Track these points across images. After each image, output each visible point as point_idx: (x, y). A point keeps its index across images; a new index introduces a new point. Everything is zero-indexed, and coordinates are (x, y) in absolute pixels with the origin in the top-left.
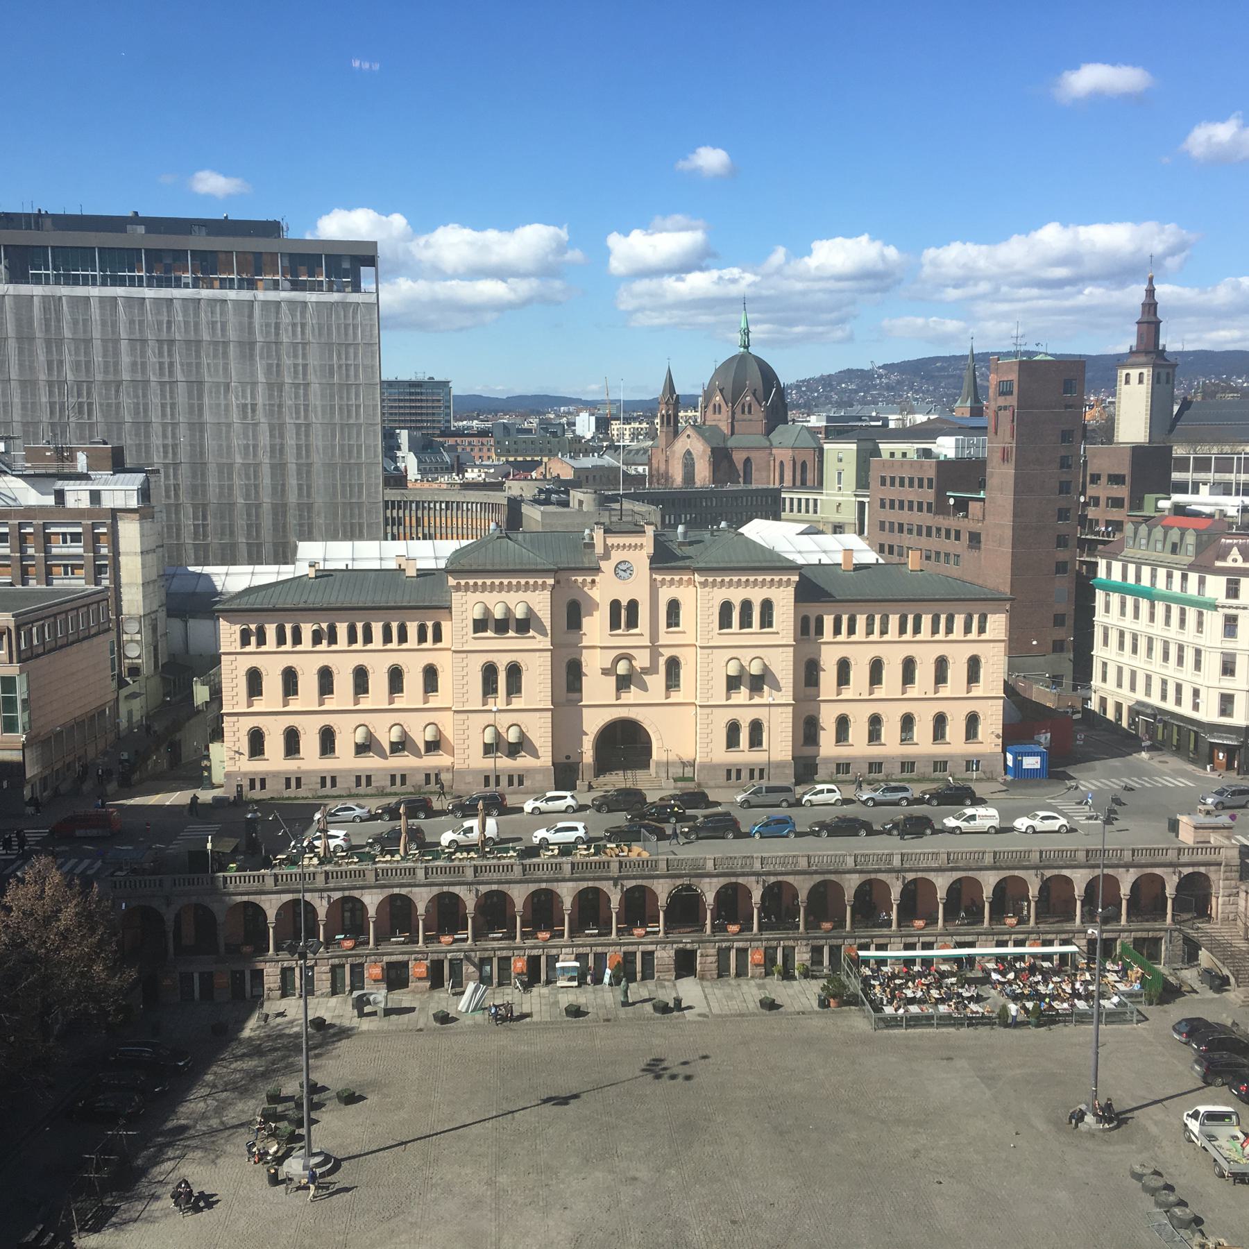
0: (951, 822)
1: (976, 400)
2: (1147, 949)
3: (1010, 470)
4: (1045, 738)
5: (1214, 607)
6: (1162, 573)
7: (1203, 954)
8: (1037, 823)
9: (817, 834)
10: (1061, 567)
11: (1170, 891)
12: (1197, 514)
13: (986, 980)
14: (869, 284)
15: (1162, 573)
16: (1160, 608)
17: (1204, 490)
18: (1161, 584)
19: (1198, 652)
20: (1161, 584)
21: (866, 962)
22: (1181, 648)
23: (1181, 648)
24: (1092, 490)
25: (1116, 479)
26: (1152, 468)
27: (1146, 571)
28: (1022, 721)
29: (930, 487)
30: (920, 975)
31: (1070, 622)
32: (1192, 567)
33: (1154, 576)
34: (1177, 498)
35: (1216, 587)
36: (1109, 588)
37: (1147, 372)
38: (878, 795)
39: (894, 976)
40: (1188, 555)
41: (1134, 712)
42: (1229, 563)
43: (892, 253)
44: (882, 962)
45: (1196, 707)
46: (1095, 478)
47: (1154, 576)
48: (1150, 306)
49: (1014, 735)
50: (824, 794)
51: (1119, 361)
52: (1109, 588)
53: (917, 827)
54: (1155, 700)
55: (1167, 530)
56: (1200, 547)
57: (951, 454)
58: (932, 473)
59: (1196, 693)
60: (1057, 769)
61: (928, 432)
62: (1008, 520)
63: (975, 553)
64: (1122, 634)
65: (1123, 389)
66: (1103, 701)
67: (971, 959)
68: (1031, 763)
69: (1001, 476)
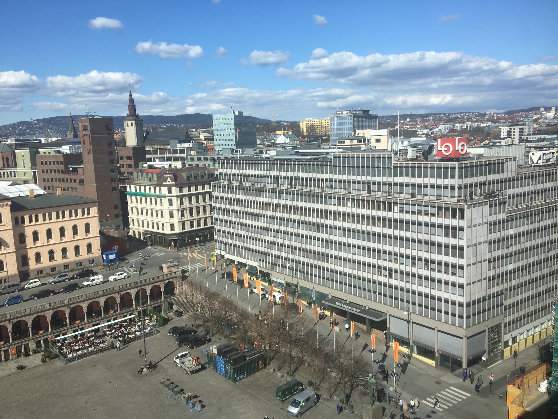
0: (86, 283)
1: (75, 132)
2: (157, 309)
4: (116, 247)
5: (165, 197)
6: (147, 188)
7: (174, 306)
8: (117, 277)
9: (33, 299)
10: (114, 189)
12: (156, 168)
13: (105, 335)
14: (26, 89)
15: (147, 188)
16: (148, 199)
17: (157, 160)
18: (148, 191)
19: (162, 212)
20: (148, 191)
21: (59, 341)
22: (157, 211)
23: (157, 211)
24: (121, 162)
25: (129, 158)
26: (139, 154)
27: (142, 187)
28: (107, 243)
29: (62, 164)
30: (80, 340)
31: (119, 207)
32: (157, 185)
33: (145, 189)
34: (149, 163)
35: (165, 190)
36: (131, 194)
37: (134, 122)
38: (56, 279)
39: (70, 343)
40: (155, 182)
42: (168, 183)
43: (34, 78)
44: (66, 339)
45: (163, 229)
46: (122, 158)
47: (145, 189)
48: (131, 100)
49: (105, 248)
50: (34, 283)
51: (124, 119)
52: (131, 194)
53: (73, 287)
54: (151, 229)
55: (147, 173)
56: (158, 178)
57: (68, 152)
59: (163, 225)
60: (122, 257)
61: (58, 144)
62: (93, 174)
65: (127, 128)
66: (134, 232)
67: (98, 330)
68: (112, 257)
69: (88, 158)
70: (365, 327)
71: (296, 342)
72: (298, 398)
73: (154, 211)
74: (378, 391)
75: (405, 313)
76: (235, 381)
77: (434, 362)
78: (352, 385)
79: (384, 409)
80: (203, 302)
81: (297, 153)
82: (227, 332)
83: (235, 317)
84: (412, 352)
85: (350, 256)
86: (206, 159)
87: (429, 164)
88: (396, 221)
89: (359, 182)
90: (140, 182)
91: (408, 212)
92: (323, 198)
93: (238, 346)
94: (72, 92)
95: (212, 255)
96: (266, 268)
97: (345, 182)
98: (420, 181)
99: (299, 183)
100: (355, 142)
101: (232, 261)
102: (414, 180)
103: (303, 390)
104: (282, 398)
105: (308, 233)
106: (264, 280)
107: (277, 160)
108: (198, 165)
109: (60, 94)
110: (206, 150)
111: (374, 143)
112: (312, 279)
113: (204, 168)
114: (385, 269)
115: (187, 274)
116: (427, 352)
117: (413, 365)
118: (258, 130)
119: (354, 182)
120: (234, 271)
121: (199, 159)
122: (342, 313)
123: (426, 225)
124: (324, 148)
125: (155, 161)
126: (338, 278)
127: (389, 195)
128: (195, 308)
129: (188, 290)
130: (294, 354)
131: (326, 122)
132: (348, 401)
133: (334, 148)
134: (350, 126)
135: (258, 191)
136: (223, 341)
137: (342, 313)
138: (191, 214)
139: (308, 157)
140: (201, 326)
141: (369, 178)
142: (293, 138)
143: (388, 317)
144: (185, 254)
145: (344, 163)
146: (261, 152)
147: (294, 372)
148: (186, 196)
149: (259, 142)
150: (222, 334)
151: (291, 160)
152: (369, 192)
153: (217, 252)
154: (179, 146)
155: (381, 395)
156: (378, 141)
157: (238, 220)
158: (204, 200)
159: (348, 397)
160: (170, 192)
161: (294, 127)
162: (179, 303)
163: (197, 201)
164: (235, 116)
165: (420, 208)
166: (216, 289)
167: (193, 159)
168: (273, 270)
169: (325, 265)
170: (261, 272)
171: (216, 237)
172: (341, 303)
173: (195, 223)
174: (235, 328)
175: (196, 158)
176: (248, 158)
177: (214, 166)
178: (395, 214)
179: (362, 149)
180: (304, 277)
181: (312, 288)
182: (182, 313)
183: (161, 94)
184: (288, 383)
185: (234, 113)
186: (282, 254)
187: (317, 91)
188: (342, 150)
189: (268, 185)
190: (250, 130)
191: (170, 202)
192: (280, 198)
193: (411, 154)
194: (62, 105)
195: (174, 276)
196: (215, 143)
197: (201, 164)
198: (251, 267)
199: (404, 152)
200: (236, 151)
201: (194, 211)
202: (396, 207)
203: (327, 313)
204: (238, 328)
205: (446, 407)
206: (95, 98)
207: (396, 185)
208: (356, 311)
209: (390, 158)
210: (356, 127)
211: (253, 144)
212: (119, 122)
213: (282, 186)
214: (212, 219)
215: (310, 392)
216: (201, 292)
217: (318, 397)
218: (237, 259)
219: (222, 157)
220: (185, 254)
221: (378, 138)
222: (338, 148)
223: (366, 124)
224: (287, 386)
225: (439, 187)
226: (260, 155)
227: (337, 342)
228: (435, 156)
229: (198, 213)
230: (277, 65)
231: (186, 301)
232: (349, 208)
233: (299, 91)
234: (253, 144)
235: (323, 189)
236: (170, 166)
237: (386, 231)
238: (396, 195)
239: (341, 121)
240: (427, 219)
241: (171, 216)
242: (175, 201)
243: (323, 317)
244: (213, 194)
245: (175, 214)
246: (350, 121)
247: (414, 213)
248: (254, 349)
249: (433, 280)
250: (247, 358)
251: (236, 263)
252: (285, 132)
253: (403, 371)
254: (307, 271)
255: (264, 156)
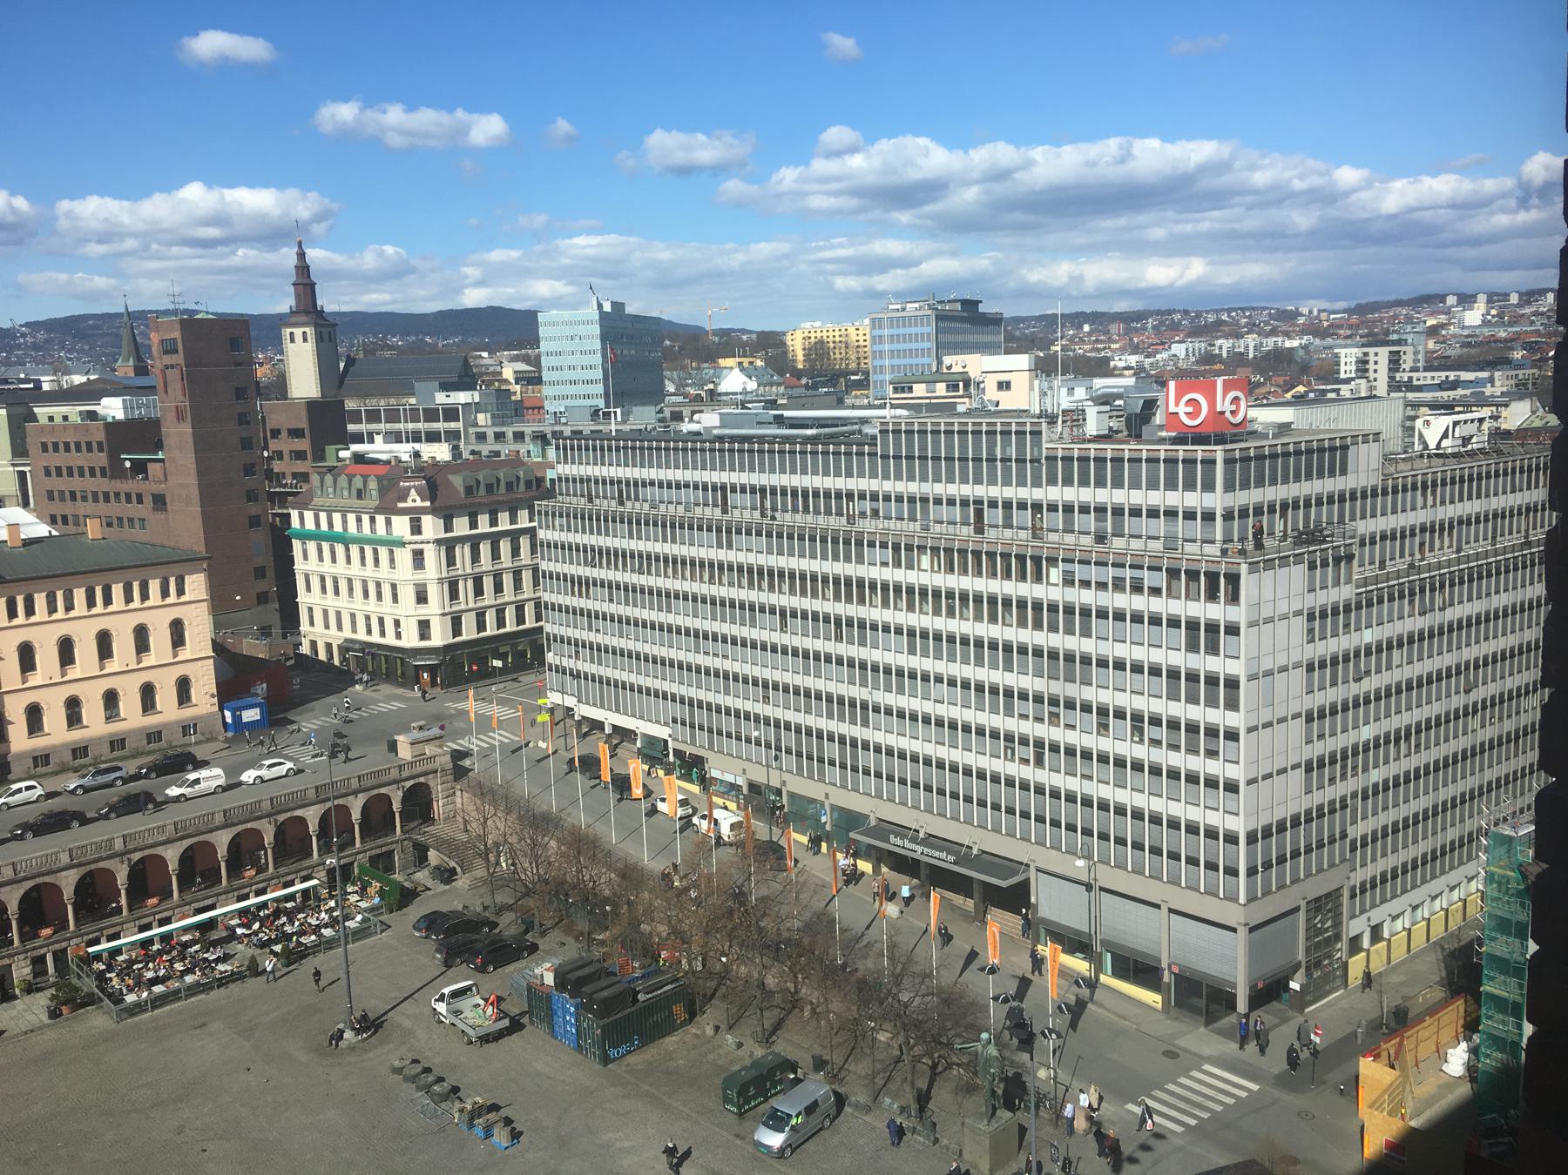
0: (174, 791)
1: (139, 358)
3: (187, 429)
4: (261, 688)
5: (403, 544)
6: (351, 518)
9: (21, 838)
10: (255, 522)
11: (396, 806)
12: (376, 462)
17: (378, 439)
19: (394, 587)
20: (352, 527)
22: (378, 585)
23: (378, 585)
24: (274, 445)
25: (296, 433)
26: (328, 422)
27: (337, 517)
28: (235, 677)
29: (101, 450)
31: (271, 573)
32: (379, 510)
33: (345, 522)
34: (355, 447)
35: (401, 525)
36: (305, 537)
37: (310, 331)
40: (373, 500)
41: (344, 649)
42: (409, 504)
43: (21, 203)
45: (398, 636)
46: (276, 433)
47: (345, 522)
48: (303, 268)
49: (230, 690)
51: (280, 321)
52: (305, 537)
53: (133, 804)
54: (361, 635)
55: (350, 478)
56: (382, 491)
57: (120, 415)
58: (100, 436)
59: (397, 623)
60: (278, 714)
62: (192, 480)
63: (161, 516)
64: (323, 579)
65: (289, 347)
66: (314, 644)
69: (179, 436)
70: (969, 904)
71: (778, 949)
72: (783, 1104)
73: (369, 583)
74: (1006, 1080)
75: (1080, 863)
76: (606, 1060)
77: (1158, 998)
78: (934, 1067)
79: (1022, 1130)
80: (513, 839)
81: (779, 421)
82: (583, 925)
83: (606, 881)
84: (1099, 969)
85: (928, 707)
86: (519, 436)
87: (1144, 450)
88: (1053, 608)
89: (951, 502)
90: (329, 502)
91: (1086, 584)
92: (852, 545)
93: (614, 963)
94: (130, 244)
95: (540, 709)
96: (693, 743)
97: (912, 500)
98: (1120, 497)
99: (784, 504)
100: (941, 389)
101: (597, 725)
102: (1103, 496)
103: (798, 1081)
104: (740, 1107)
105: (809, 643)
106: (686, 777)
107: (721, 439)
108: (497, 454)
109: (96, 249)
110: (519, 410)
111: (992, 393)
112: (821, 772)
113: (515, 461)
114: (1024, 741)
115: (467, 763)
116: (1139, 969)
117: (1101, 1006)
118: (669, 355)
119: (938, 501)
120: (603, 751)
121: (499, 436)
122: (905, 865)
123: (1137, 618)
124: (853, 407)
125: (371, 441)
126: (894, 770)
127: (1035, 536)
128: (492, 857)
129: (472, 808)
130: (771, 981)
131: (859, 332)
132: (922, 1109)
133: (882, 407)
134: (926, 345)
135: (671, 528)
136: (572, 951)
137: (905, 865)
138: (479, 591)
139: (809, 432)
140: (509, 908)
141: (981, 491)
142: (766, 378)
143: (1032, 874)
144: (461, 706)
145: (908, 450)
146: (677, 417)
147: (773, 1033)
148: (462, 540)
149: (671, 388)
150: (568, 930)
151: (761, 439)
152: (979, 530)
153: (554, 698)
154: (441, 398)
155: (1014, 1092)
156: (1004, 386)
157: (612, 608)
158: (515, 552)
159: (923, 1099)
160: (416, 528)
161: (769, 345)
162: (445, 845)
163: (496, 555)
164: (603, 316)
165: (1119, 572)
166: (551, 802)
167: (481, 437)
168: (711, 748)
169: (857, 732)
170: (678, 753)
171: (550, 657)
172: (903, 837)
173: (490, 617)
174: (605, 913)
175: (490, 433)
176: (640, 435)
177: (544, 455)
178: (1051, 590)
179: (961, 409)
180: (799, 768)
181: (821, 797)
182: (453, 872)
183: (389, 250)
184: (755, 1064)
185: (600, 306)
186: (739, 704)
187: (832, 247)
188: (904, 412)
189: (699, 510)
190: (644, 355)
191: (418, 557)
192: (730, 547)
193: (1094, 423)
194: (100, 282)
195: (430, 767)
196: (547, 391)
197: (506, 450)
198: (651, 741)
199: (1075, 417)
200: (607, 415)
201: (488, 583)
202: (1053, 571)
203: (865, 866)
204: (616, 913)
205: (1193, 1122)
206: (196, 262)
207: (1053, 508)
208: (944, 859)
209: (1036, 434)
210: (942, 348)
211: (655, 395)
212: (269, 330)
213: (736, 513)
214: (538, 605)
215: (816, 1088)
216: (508, 811)
217: (840, 1100)
218: (611, 718)
219: (567, 431)
220: (461, 706)
221: (1004, 377)
222: (893, 407)
223: (970, 338)
224: (754, 1073)
225: (1171, 513)
226: (673, 426)
227: (893, 946)
228: (1161, 427)
229: (498, 588)
230: (720, 170)
231: (463, 837)
232: (926, 574)
233: (785, 247)
234: (655, 395)
235: (851, 519)
236: (417, 455)
237: (1028, 636)
238: (1053, 537)
239: (901, 331)
240: (1140, 603)
241: (422, 598)
242: (430, 554)
243: (853, 877)
244: (542, 534)
245: (433, 592)
246: (926, 330)
247: (1102, 586)
248: (659, 971)
249: (1155, 771)
250: (641, 997)
251: (608, 730)
252: (746, 361)
253: (1073, 1025)
254: (807, 749)
255: (686, 427)
